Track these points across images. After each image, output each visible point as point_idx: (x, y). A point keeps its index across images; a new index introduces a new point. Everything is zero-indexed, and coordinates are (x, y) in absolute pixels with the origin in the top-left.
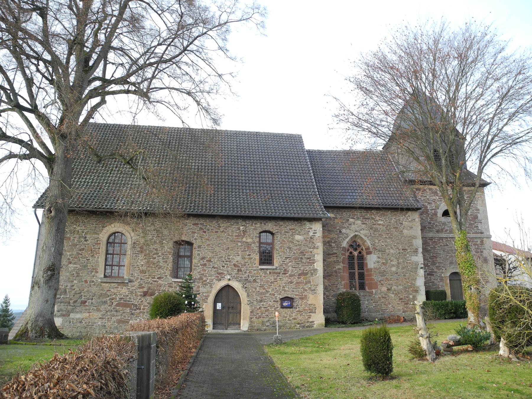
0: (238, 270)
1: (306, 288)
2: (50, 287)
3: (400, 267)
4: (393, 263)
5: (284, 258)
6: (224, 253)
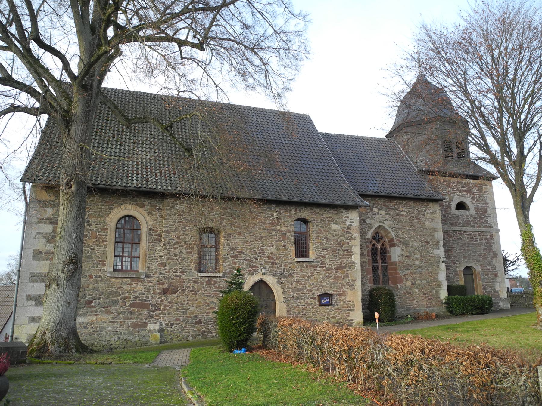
0: (273, 262)
1: (344, 284)
2: (72, 284)
3: (424, 261)
4: (416, 256)
5: (321, 250)
6: (257, 243)
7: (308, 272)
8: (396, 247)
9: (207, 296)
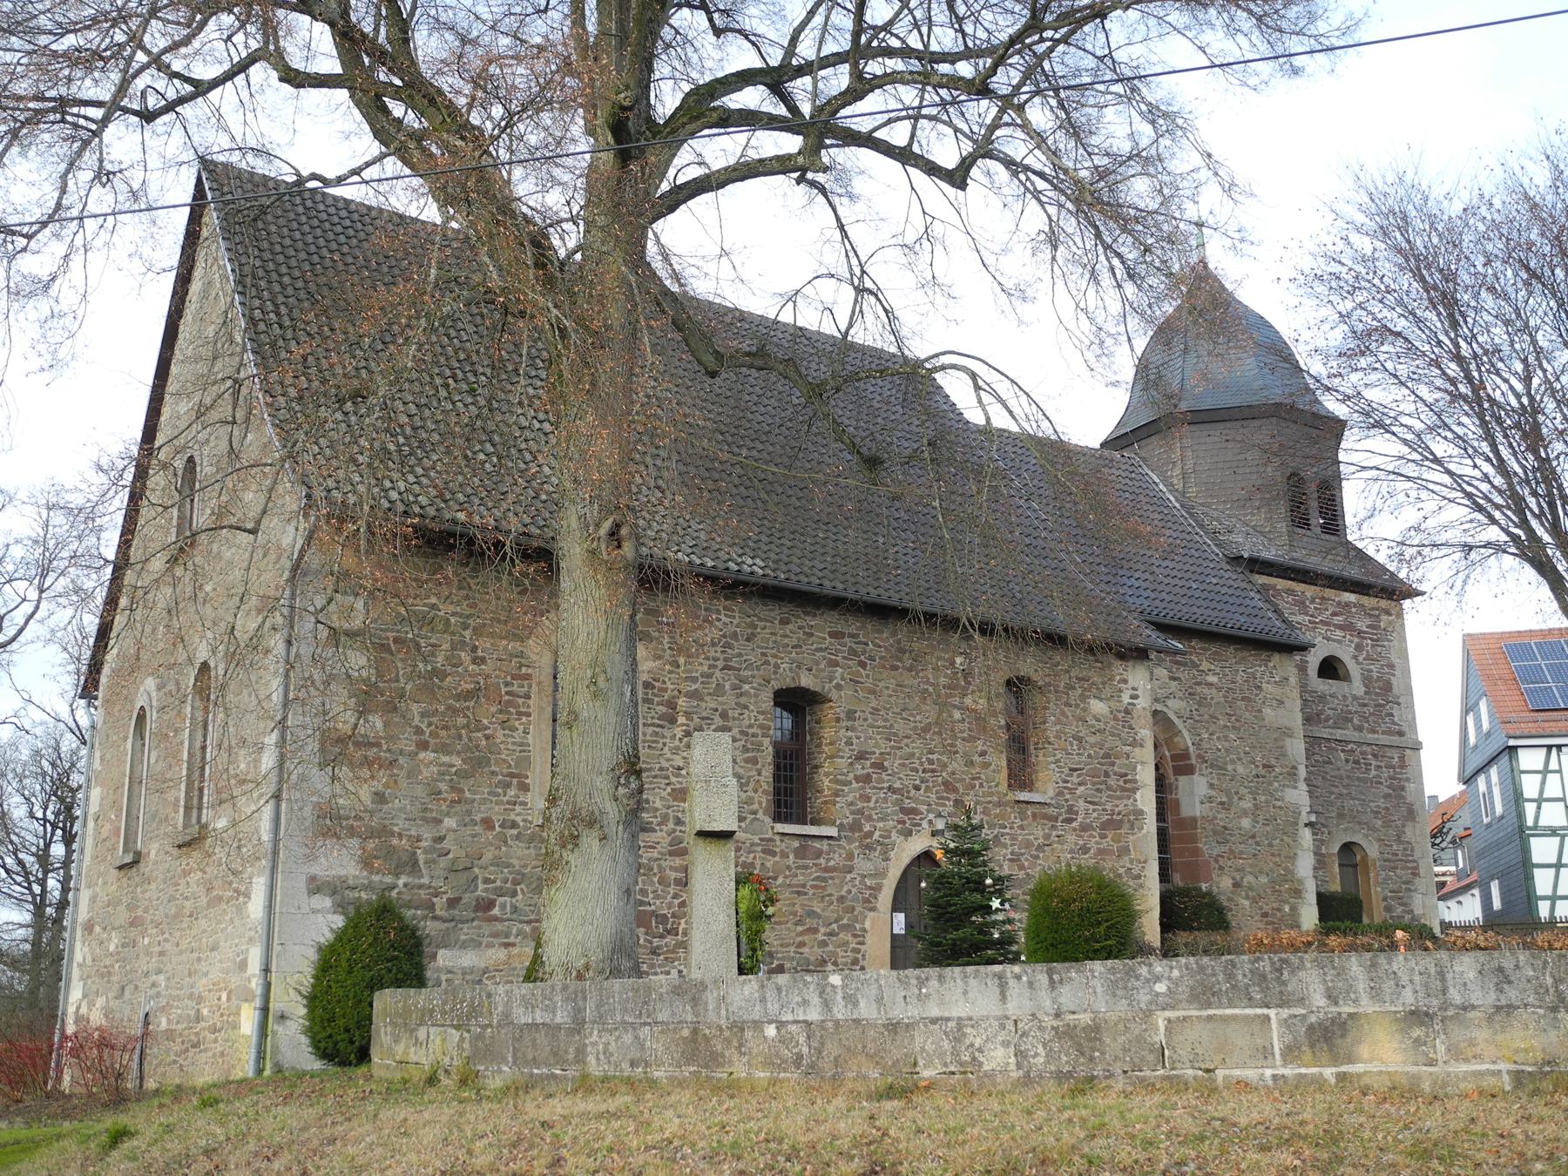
5: (1066, 771)
7: (1037, 833)
8: (1195, 777)
9: (798, 893)
